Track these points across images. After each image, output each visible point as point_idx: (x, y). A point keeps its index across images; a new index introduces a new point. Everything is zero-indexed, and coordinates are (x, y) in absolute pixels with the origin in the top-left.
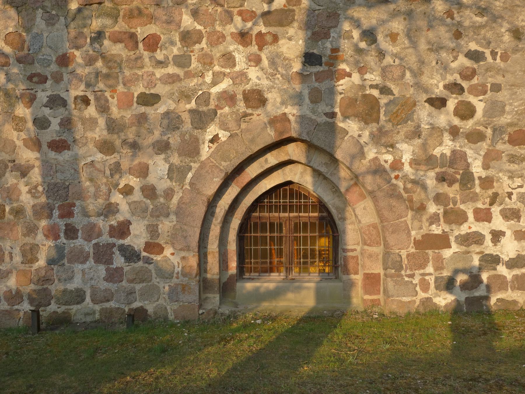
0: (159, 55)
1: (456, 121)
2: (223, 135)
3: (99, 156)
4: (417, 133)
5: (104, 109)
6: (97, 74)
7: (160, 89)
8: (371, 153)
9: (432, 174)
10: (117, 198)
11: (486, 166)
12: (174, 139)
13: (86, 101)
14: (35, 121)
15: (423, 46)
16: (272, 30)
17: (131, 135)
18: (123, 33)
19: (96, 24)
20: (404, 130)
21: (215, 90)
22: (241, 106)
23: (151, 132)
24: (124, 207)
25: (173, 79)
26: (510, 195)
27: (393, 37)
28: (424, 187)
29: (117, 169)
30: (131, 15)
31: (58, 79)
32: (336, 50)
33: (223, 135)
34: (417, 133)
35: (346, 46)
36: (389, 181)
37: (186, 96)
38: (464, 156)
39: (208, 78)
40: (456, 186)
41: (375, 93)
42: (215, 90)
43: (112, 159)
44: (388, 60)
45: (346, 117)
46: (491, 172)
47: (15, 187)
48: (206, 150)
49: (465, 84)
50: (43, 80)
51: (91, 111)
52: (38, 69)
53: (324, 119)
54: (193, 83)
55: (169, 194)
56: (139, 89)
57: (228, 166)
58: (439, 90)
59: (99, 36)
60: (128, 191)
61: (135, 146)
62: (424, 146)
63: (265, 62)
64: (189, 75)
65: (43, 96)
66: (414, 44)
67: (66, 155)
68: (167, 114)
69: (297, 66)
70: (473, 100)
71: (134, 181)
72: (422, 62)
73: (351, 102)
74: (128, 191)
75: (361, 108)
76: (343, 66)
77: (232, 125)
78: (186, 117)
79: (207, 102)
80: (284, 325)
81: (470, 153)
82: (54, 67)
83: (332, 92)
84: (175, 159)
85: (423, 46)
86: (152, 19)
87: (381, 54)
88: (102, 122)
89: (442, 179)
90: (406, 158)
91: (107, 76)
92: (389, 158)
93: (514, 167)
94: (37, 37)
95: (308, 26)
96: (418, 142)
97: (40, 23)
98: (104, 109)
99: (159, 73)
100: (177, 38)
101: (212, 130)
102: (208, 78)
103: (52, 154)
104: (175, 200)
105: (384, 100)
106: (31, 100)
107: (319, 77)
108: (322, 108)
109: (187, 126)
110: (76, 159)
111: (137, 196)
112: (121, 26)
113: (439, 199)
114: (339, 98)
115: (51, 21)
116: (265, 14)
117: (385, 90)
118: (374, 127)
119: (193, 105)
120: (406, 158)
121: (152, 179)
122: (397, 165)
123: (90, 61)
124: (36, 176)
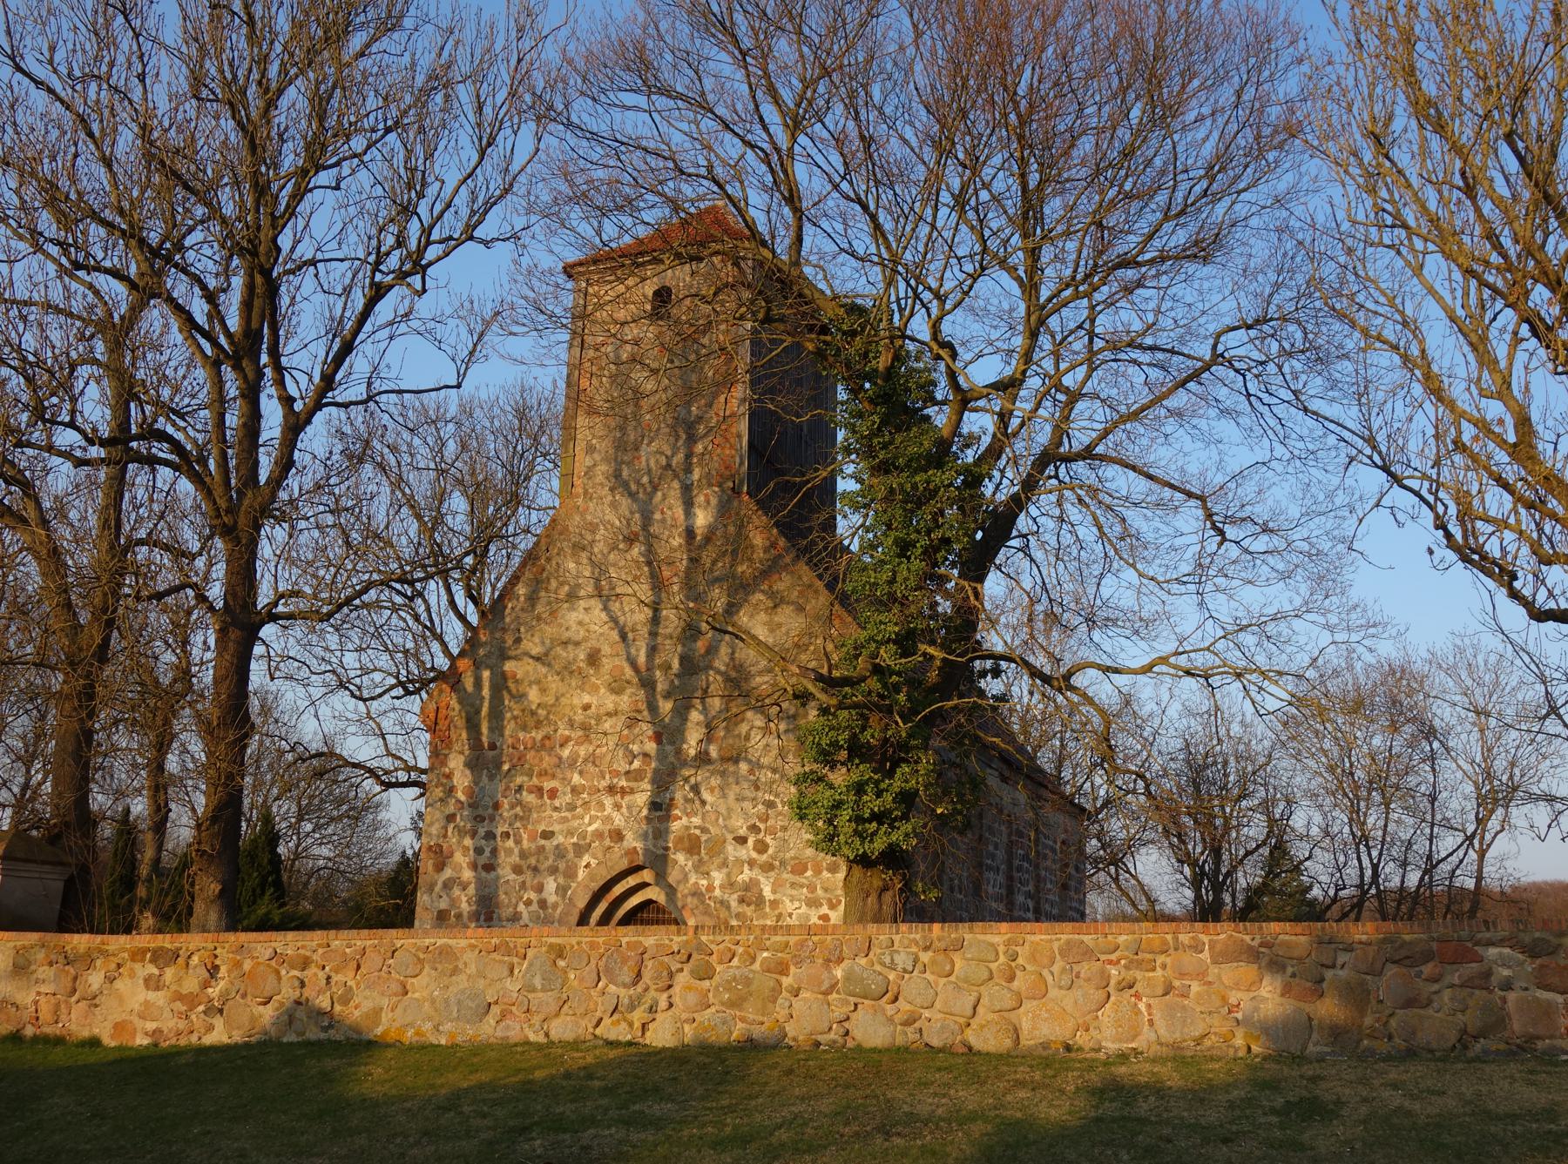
0: (557, 803)
1: (754, 855)
2: (594, 862)
3: (512, 877)
4: (724, 864)
5: (518, 842)
6: (516, 816)
7: (556, 828)
8: (693, 879)
9: (735, 896)
10: (521, 907)
11: (774, 892)
12: (562, 866)
13: (507, 835)
14: (494, 837)
15: (731, 796)
16: (631, 784)
17: (533, 861)
18: (615, 606)
19: (519, 780)
20: (717, 861)
21: (590, 829)
22: (607, 842)
23: (547, 858)
24: (525, 916)
25: (565, 820)
26: (790, 915)
27: (712, 790)
28: (728, 908)
29: (523, 885)
30: (540, 775)
31: (492, 819)
32: (672, 799)
33: (594, 862)
34: (724, 864)
35: (679, 796)
36: (703, 902)
37: (570, 833)
38: (757, 883)
39: (587, 820)
40: (752, 907)
41: (698, 832)
42: (590, 829)
43: (520, 879)
44: (708, 807)
45: (677, 850)
46: (778, 896)
47: (459, 897)
48: (581, 874)
49: (762, 826)
50: (483, 820)
51: (510, 843)
52: (480, 812)
53: (660, 852)
54: (576, 823)
55: (555, 906)
56: (541, 828)
57: (596, 886)
58: (742, 832)
59: (520, 789)
60: (528, 903)
61: (535, 869)
62: (728, 875)
63: (624, 810)
64: (574, 818)
65: (482, 832)
66: (724, 796)
67: (493, 874)
68: (557, 847)
69: (645, 812)
70: (768, 839)
71: (533, 895)
72: (729, 810)
73: (680, 840)
74: (528, 903)
75: (687, 844)
76: (677, 812)
77: (600, 855)
78: (570, 848)
79: (584, 838)
80: (645, 1050)
81: (762, 880)
82: (490, 811)
83: (667, 831)
84: (561, 880)
85: (731, 796)
86: (554, 776)
87: (703, 803)
88: (516, 851)
89: (742, 901)
90: (717, 883)
91: (522, 818)
92: (704, 882)
93: (794, 892)
94: (483, 788)
95: (653, 782)
96: (725, 870)
97: (485, 779)
98: (518, 842)
99: (555, 815)
100: (568, 789)
101: (586, 859)
102: (587, 820)
103: (484, 874)
104: (559, 911)
105: (704, 838)
106: (474, 834)
107: (660, 819)
108: (661, 843)
109: (571, 855)
110: (498, 878)
111: (535, 907)
112: (535, 781)
113: (738, 916)
114: (672, 837)
115: (491, 778)
116: (628, 773)
117: (704, 830)
118: (696, 857)
119: (575, 840)
120: (717, 883)
121: (544, 895)
122: (710, 888)
123: (512, 807)
124: (471, 890)
